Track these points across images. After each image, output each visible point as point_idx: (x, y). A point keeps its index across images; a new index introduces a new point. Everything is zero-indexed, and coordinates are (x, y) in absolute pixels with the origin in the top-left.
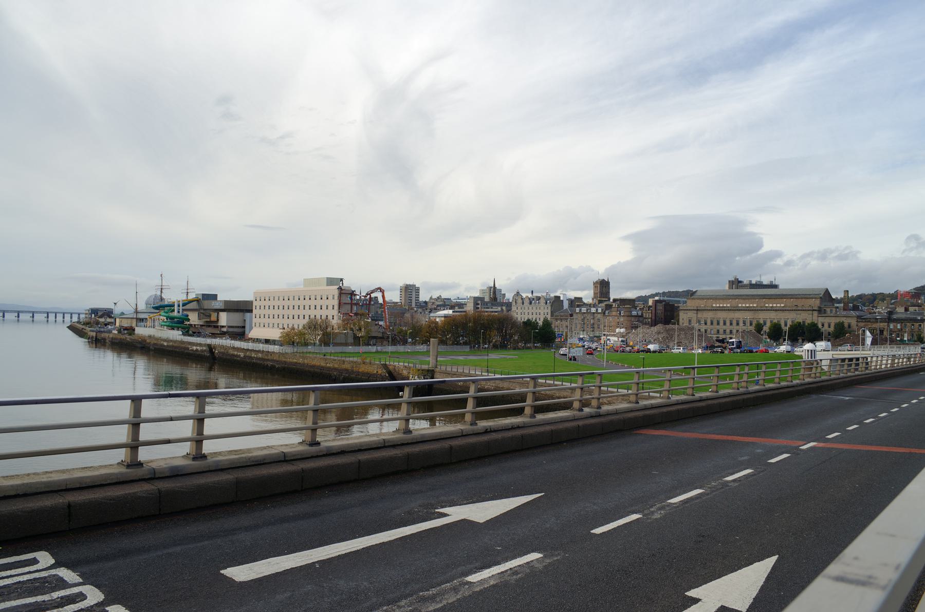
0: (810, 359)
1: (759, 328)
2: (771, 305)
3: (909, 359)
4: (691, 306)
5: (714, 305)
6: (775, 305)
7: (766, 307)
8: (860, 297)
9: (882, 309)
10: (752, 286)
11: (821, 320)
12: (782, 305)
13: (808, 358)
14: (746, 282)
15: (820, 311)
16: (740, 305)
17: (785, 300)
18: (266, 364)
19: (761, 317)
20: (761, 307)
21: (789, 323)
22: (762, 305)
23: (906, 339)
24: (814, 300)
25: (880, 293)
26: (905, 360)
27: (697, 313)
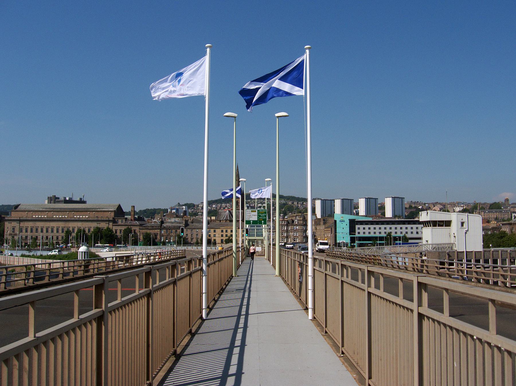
0: (86, 259)
1: (68, 233)
2: (78, 217)
3: (148, 257)
4: (14, 217)
5: (34, 216)
6: (81, 217)
7: (75, 218)
8: (145, 211)
9: (158, 220)
10: (66, 202)
11: (114, 228)
12: (87, 217)
13: (82, 258)
14: (62, 198)
15: (114, 221)
16: (55, 217)
17: (89, 212)
18: (49, 254)
19: (71, 225)
20: (71, 218)
21: (92, 230)
22: (72, 216)
23: (172, 241)
24: (110, 213)
25: (159, 209)
26: (144, 259)
27: (20, 223)
